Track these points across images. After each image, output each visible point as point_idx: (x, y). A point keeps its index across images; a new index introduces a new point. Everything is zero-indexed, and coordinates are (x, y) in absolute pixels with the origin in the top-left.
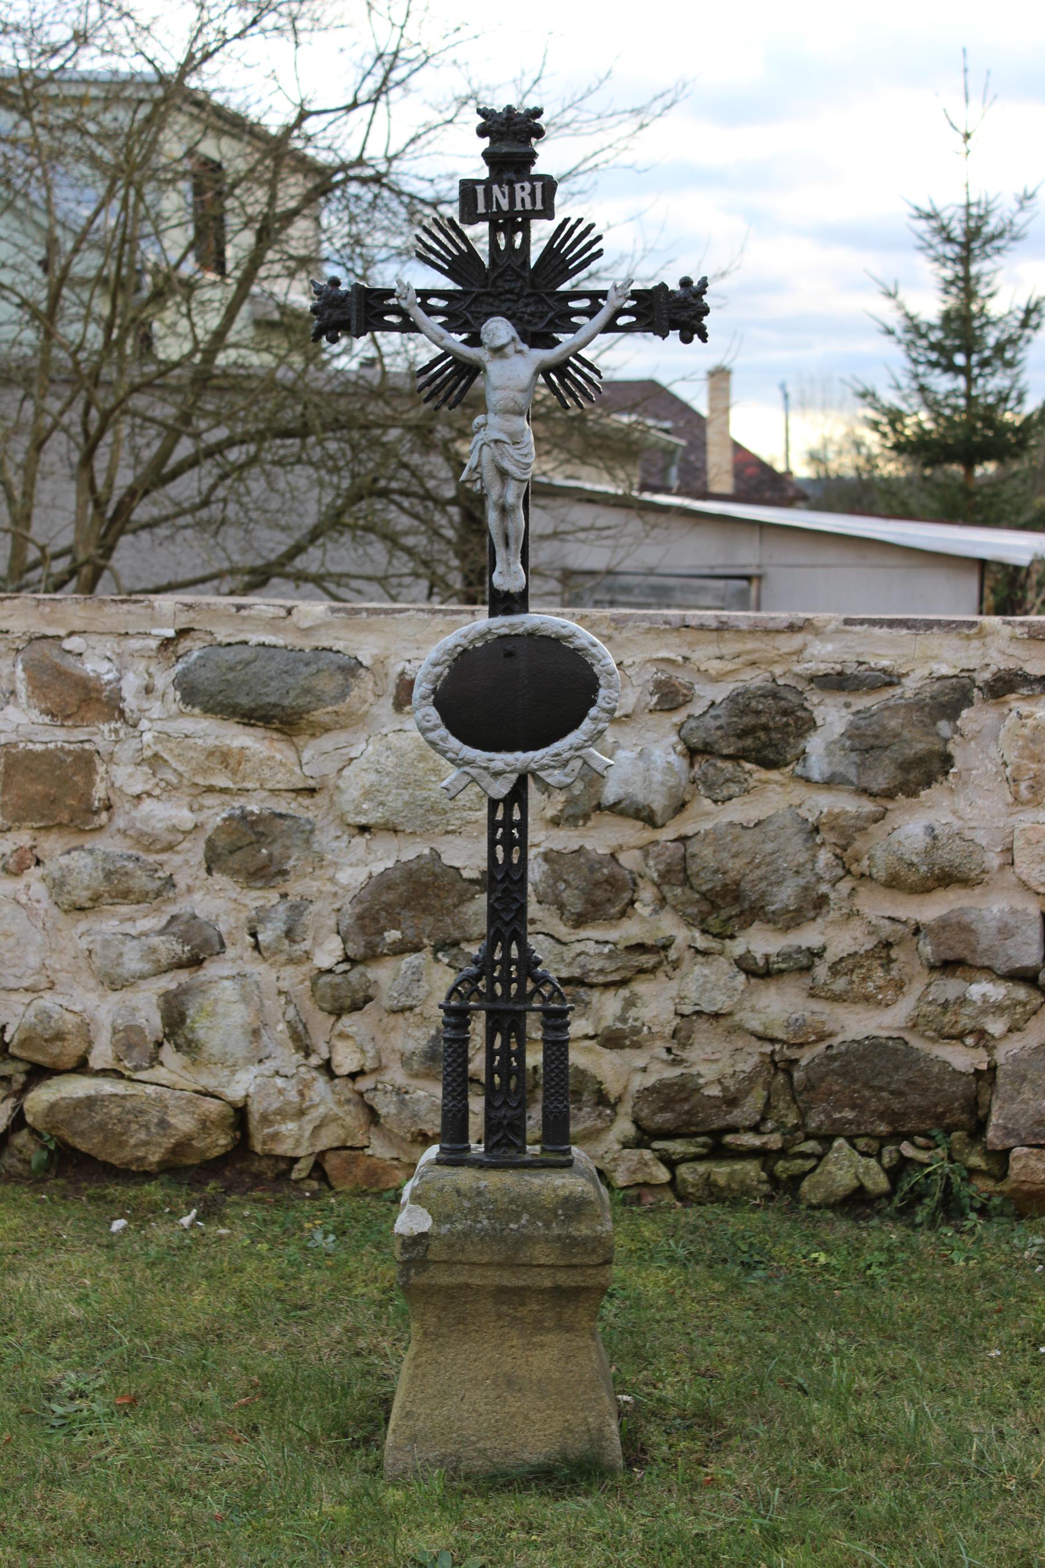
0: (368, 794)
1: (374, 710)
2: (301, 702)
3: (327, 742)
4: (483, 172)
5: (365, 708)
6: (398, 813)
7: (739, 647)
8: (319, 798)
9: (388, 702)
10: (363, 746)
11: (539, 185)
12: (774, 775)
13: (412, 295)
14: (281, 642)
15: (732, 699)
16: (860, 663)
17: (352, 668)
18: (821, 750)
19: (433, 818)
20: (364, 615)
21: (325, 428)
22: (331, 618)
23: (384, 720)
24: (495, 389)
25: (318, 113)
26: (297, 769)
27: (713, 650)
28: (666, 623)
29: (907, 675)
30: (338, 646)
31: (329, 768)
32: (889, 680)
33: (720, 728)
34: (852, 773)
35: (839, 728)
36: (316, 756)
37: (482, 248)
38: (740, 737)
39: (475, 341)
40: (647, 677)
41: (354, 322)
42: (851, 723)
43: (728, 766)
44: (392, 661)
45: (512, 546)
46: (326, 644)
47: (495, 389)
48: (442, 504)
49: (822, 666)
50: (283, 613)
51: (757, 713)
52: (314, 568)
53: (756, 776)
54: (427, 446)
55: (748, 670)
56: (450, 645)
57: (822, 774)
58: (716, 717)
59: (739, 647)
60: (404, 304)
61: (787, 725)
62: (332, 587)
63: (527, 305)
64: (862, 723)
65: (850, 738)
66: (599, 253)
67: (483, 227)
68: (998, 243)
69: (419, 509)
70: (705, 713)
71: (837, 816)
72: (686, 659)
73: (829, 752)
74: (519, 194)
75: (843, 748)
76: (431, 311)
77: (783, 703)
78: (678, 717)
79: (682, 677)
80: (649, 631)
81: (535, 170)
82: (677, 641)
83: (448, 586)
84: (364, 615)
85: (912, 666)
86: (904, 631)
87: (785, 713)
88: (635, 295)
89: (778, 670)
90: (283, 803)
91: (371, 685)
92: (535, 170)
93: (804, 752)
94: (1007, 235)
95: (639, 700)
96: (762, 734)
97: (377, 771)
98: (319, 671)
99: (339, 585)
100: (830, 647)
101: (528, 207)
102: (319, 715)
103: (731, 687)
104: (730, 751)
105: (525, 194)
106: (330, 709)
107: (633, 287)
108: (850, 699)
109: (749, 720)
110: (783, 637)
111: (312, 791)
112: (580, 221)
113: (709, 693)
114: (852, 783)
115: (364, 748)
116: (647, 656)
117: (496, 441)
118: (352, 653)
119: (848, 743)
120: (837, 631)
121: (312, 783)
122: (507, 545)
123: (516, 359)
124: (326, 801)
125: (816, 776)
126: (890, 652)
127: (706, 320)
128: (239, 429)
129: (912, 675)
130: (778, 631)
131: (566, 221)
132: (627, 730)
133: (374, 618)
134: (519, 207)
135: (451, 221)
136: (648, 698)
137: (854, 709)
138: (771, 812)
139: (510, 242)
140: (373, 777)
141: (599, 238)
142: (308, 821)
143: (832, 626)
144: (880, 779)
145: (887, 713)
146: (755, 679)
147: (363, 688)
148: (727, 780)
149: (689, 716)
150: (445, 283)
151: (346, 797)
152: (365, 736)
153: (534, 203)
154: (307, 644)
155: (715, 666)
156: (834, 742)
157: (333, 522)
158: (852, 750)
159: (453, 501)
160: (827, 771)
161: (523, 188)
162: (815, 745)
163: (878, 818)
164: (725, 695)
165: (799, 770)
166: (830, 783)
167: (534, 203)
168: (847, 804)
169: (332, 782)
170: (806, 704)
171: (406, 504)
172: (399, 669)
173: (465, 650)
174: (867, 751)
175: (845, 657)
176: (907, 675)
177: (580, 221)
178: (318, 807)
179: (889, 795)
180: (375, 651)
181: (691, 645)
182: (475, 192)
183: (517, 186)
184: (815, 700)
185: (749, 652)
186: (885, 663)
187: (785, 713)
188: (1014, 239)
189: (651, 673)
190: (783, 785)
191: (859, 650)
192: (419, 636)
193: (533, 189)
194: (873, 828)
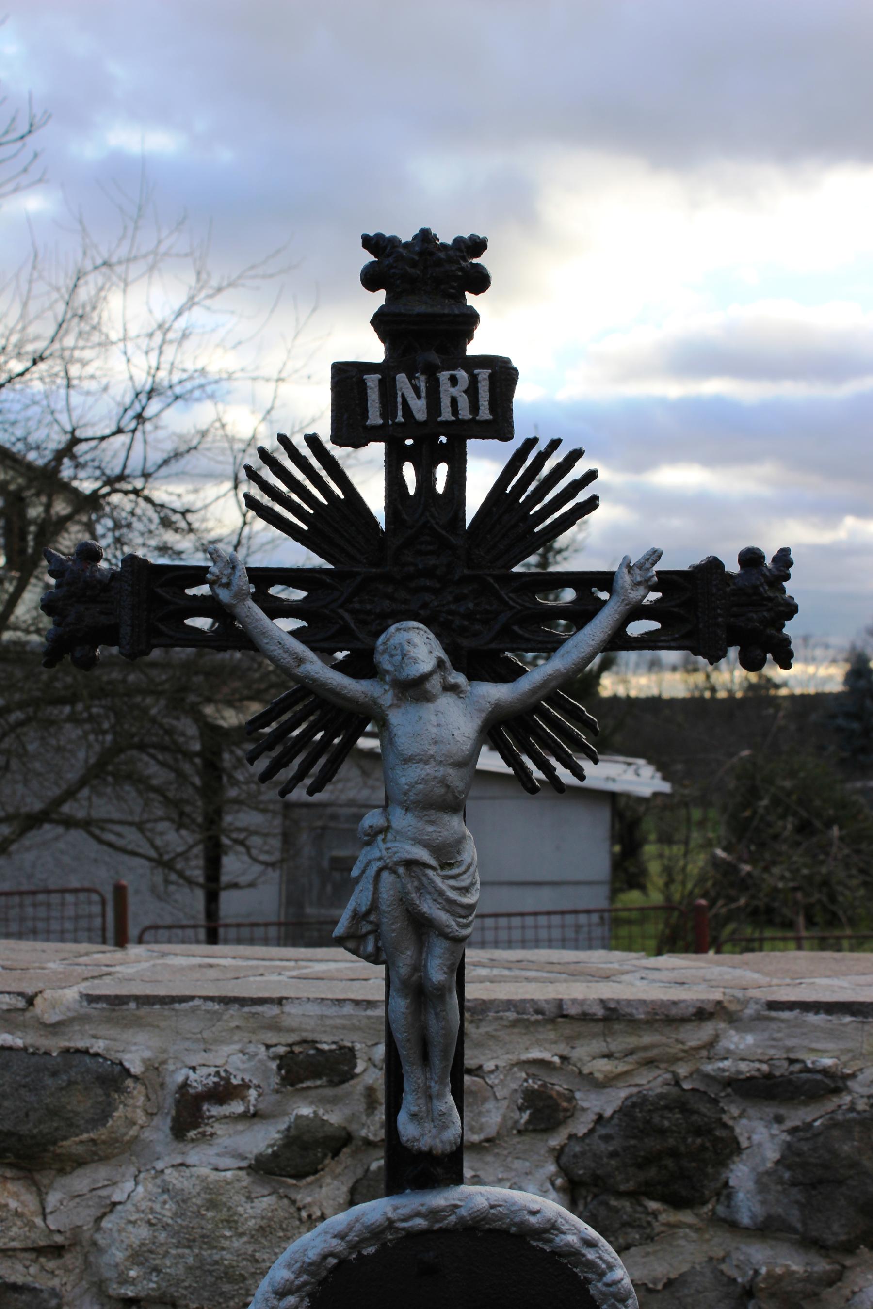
0: (137, 1256)
1: (147, 1135)
2: (45, 1128)
3: (80, 1181)
4: (372, 350)
5: (133, 1132)
6: (178, 1283)
7: (632, 1041)
8: (69, 1258)
9: (165, 1124)
10: (129, 1185)
11: (484, 374)
12: (686, 1217)
13: (242, 580)
14: (19, 1043)
15: (626, 1111)
16: (792, 1061)
17: (114, 1078)
18: (750, 1185)
19: (226, 1287)
20: (133, 1005)
21: (92, 697)
22: (87, 1009)
23: (159, 1149)
24: (408, 760)
25: (87, 440)
26: (38, 1221)
27: (598, 1046)
28: (538, 1012)
29: (853, 1076)
30: (98, 1046)
31: (84, 1217)
32: (832, 1083)
33: (613, 1155)
34: (795, 1217)
35: (772, 1154)
36: (64, 1203)
37: (374, 495)
38: (640, 1166)
39: (362, 666)
40: (514, 1086)
41: (125, 631)
42: (789, 1146)
43: (626, 1205)
44: (171, 1067)
45: (436, 1061)
46: (81, 1044)
47: (408, 760)
48: (189, 756)
49: (744, 1066)
50: (21, 1003)
51: (662, 1132)
52: (81, 814)
53: (663, 1218)
54: (445, 1168)
55: (644, 1071)
56: (313, 1255)
57: (753, 1217)
58: (607, 1138)
59: (632, 1041)
60: (224, 595)
61: (703, 1148)
62: (97, 832)
63: (457, 599)
64: (805, 1147)
65: (789, 1167)
66: (592, 504)
67: (376, 450)
68: (565, 554)
69: (171, 761)
70: (591, 1131)
71: (780, 1278)
72: (563, 1058)
73: (761, 1184)
74: (447, 391)
75: (781, 1182)
76: (277, 609)
77: (695, 1118)
78: (555, 1141)
79: (559, 1085)
80: (515, 1024)
81: (473, 349)
82: (552, 1035)
83: (194, 821)
84: (133, 1005)
85: (858, 1064)
86: (848, 1019)
87: (698, 1131)
88: (668, 581)
89: (682, 1070)
90: (19, 1267)
91: (142, 1099)
92: (473, 349)
93: (726, 1184)
94: (571, 549)
95: (505, 1117)
96: (670, 1163)
97: (150, 1223)
98: (70, 1083)
99: (103, 829)
100: (750, 1039)
101: (465, 413)
102: (71, 1145)
103: (623, 1094)
104: (631, 1186)
105: (458, 392)
106: (85, 1136)
107: (659, 567)
108: (782, 1111)
109: (653, 1144)
110: (689, 1026)
111: (57, 1251)
112: (555, 444)
113: (596, 1104)
114: (795, 1231)
115: (132, 1190)
116: (513, 1058)
117: (411, 864)
118: (114, 1056)
119: (787, 1175)
120: (758, 1018)
121: (59, 1239)
122: (425, 1058)
123: (446, 703)
124: (79, 1262)
125: (745, 1219)
126: (830, 1046)
127: (790, 628)
128: (17, 697)
129: (860, 1077)
130: (684, 1020)
131: (530, 443)
132: (489, 1158)
133: (145, 1010)
134: (446, 415)
135: (313, 441)
136: (516, 1115)
137: (789, 1124)
138: (685, 1268)
139: (426, 479)
140: (144, 1232)
141: (591, 476)
142: (54, 1293)
143: (749, 1011)
144: (835, 1227)
145: (835, 1133)
146: (652, 1082)
147: (132, 1109)
148: (625, 1224)
149: (571, 1137)
150: (297, 555)
151: (106, 1259)
152: (133, 1170)
153: (474, 407)
154: (55, 1044)
155: (602, 1067)
156: (768, 1173)
157: (97, 773)
158: (794, 1184)
159: (197, 754)
160: (759, 1210)
161: (454, 381)
162: (741, 1175)
163: (833, 1280)
164: (616, 1104)
165: (721, 1210)
166: (766, 1229)
167: (474, 407)
168: (787, 1261)
169: (87, 1235)
170: (725, 1118)
171: (160, 757)
172: (180, 1078)
173: (343, 1262)
174: (813, 1186)
175: (772, 1052)
176: (853, 1076)
177: (555, 444)
178: (67, 1270)
179: (849, 1248)
180: (147, 1054)
181: (570, 1040)
182: (363, 385)
183: (444, 376)
184: (735, 1111)
185: (645, 1048)
186: (827, 1062)
187: (698, 1131)
188: (576, 551)
189: (519, 1080)
190: (697, 1230)
191: (790, 1043)
192: (206, 1034)
193: (474, 381)
194: (827, 1293)
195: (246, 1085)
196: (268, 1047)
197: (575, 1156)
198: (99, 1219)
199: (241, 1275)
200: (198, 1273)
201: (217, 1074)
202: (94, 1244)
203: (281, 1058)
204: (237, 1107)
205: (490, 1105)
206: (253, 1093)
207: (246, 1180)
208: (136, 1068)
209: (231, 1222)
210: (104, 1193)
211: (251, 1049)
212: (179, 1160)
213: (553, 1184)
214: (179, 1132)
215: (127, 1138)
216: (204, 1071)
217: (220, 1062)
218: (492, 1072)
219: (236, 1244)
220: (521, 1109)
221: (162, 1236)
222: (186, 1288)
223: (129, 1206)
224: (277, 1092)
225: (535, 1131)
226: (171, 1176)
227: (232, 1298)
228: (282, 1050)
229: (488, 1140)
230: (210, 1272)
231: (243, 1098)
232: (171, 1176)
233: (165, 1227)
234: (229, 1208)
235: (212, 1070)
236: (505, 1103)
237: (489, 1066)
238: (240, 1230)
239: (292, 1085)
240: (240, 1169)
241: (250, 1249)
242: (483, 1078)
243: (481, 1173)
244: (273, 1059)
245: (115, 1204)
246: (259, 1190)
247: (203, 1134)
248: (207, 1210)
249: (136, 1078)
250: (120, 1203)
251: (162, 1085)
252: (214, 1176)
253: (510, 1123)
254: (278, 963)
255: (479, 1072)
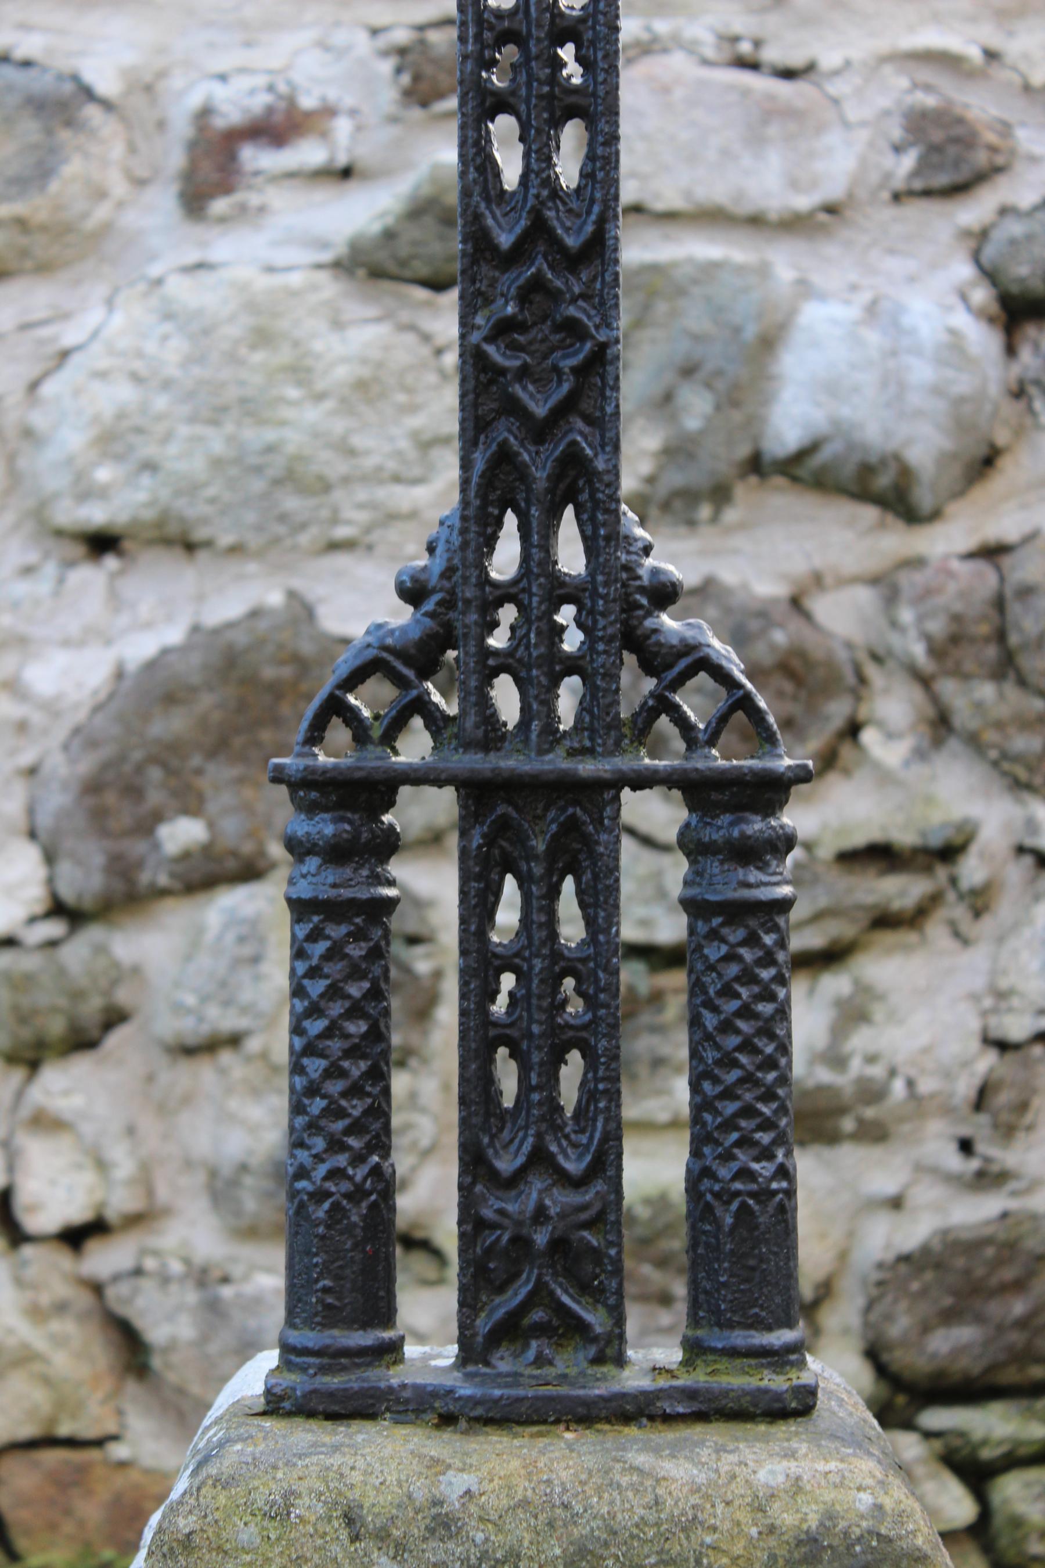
0: (112, 439)
1: (130, 219)
5: (102, 212)
6: (192, 489)
10: (94, 316)
40: (884, 102)
72: (991, 55)
78: (974, 211)
79: (980, 105)
95: (863, 163)
97: (136, 378)
116: (883, 44)
118: (63, 64)
136: (889, 161)
140: (125, 393)
147: (97, 165)
149: (1004, 211)
151: (51, 454)
152: (101, 290)
172: (195, 100)
180: (130, 58)
189: (896, 90)
195: (329, 111)
196: (375, 32)
197: (1013, 242)
198: (34, 386)
199: (320, 478)
200: (233, 471)
201: (271, 88)
202: (28, 433)
203: (402, 51)
204: (309, 153)
205: (833, 138)
206: (342, 127)
207: (329, 287)
208: (106, 85)
209: (299, 372)
210: (45, 332)
211: (340, 37)
212: (193, 256)
213: (964, 297)
214: (195, 200)
215: (90, 224)
216: (241, 84)
217: (276, 63)
218: (836, 73)
219: (312, 414)
220: (898, 149)
221: (161, 402)
222: (212, 501)
223: (96, 347)
224: (393, 120)
225: (927, 193)
226: (178, 287)
227: (303, 526)
228: (401, 36)
229: (831, 209)
230: (258, 470)
231: (324, 135)
232: (178, 287)
233: (167, 385)
234: (296, 344)
235: (261, 80)
236: (863, 135)
237: (829, 59)
238: (320, 385)
239: (424, 104)
240: (319, 266)
241: (339, 426)
242: (818, 85)
243: (817, 279)
244: (385, 53)
245: (65, 355)
246: (355, 309)
247: (243, 209)
248: (253, 347)
249: (107, 105)
250: (78, 348)
251: (161, 125)
252: (263, 282)
253: (874, 177)
254: (425, 1100)
255: (813, 76)
